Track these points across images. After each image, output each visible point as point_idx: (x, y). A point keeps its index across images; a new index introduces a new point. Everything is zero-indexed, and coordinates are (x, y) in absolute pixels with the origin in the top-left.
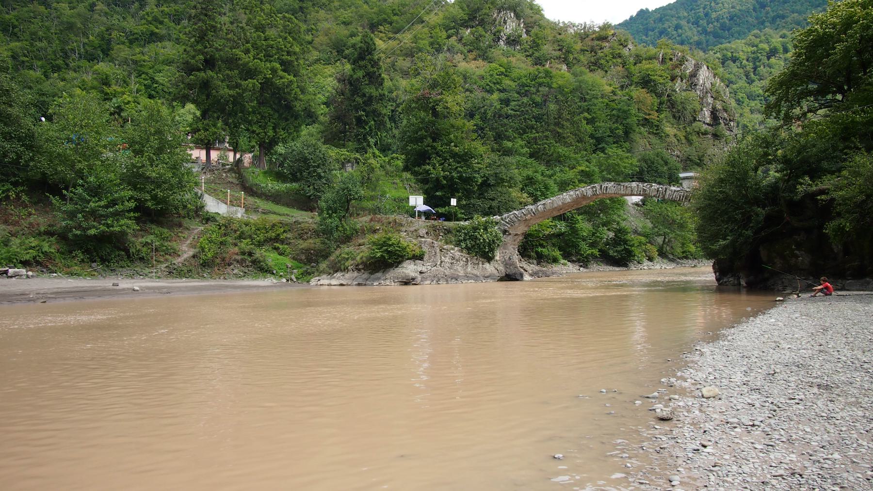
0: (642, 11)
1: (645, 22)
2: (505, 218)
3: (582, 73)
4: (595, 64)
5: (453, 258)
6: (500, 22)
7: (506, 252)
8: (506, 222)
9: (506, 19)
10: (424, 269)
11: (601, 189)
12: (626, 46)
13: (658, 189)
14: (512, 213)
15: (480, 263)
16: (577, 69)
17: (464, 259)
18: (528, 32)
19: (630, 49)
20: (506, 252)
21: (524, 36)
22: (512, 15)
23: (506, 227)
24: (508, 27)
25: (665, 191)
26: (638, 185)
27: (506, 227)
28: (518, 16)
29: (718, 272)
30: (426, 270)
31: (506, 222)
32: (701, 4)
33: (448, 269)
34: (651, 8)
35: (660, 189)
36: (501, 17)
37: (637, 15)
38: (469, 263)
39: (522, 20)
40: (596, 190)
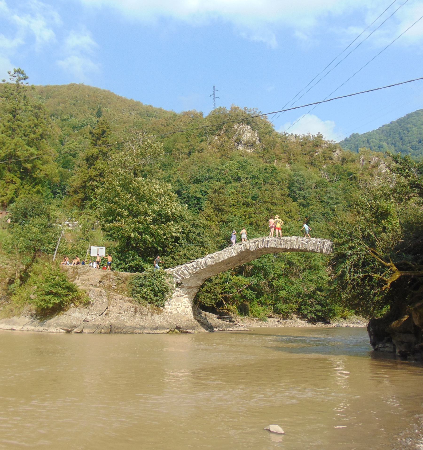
0: (353, 135)
1: (356, 143)
2: (177, 271)
3: (300, 170)
4: (312, 164)
5: (121, 308)
6: (239, 132)
7: (179, 305)
8: (178, 274)
9: (244, 130)
10: (89, 318)
11: (263, 243)
12: (335, 151)
13: (316, 242)
14: (184, 266)
15: (149, 314)
16: (297, 166)
17: (133, 310)
18: (260, 140)
19: (338, 154)
20: (179, 305)
21: (258, 143)
22: (249, 127)
23: (178, 280)
24: (246, 136)
25: (323, 245)
26: (297, 239)
27: (178, 280)
28: (253, 129)
29: (372, 335)
30: (90, 319)
31: (178, 274)
32: (397, 131)
33: (115, 319)
34: (361, 133)
35: (318, 243)
36: (241, 129)
37: (350, 137)
38: (138, 314)
39: (256, 131)
40: (258, 245)
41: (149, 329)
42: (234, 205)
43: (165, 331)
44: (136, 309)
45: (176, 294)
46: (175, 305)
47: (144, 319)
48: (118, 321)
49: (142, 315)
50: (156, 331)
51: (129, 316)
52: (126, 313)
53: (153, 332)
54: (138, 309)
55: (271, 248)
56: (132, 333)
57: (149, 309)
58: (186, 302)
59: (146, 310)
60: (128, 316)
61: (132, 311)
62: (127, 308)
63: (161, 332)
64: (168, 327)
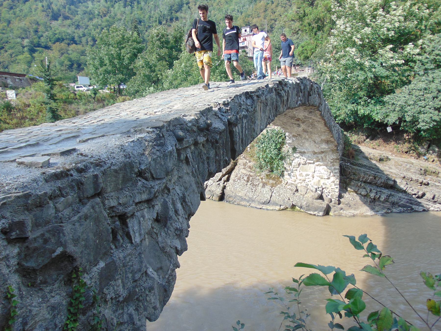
38: (249, 184)
41: (257, 203)
42: (233, 11)
43: (278, 208)
44: (248, 178)
45: (296, 161)
46: (301, 175)
47: (253, 191)
48: (412, 134)
49: (253, 185)
50: (264, 207)
51: (241, 185)
52: (239, 181)
53: (261, 207)
54: (251, 178)
55: (243, 151)
56: (238, 204)
57: (262, 179)
58: (323, 171)
59: (259, 179)
60: (240, 184)
61: (244, 180)
62: (241, 176)
63: (271, 208)
64: (281, 203)
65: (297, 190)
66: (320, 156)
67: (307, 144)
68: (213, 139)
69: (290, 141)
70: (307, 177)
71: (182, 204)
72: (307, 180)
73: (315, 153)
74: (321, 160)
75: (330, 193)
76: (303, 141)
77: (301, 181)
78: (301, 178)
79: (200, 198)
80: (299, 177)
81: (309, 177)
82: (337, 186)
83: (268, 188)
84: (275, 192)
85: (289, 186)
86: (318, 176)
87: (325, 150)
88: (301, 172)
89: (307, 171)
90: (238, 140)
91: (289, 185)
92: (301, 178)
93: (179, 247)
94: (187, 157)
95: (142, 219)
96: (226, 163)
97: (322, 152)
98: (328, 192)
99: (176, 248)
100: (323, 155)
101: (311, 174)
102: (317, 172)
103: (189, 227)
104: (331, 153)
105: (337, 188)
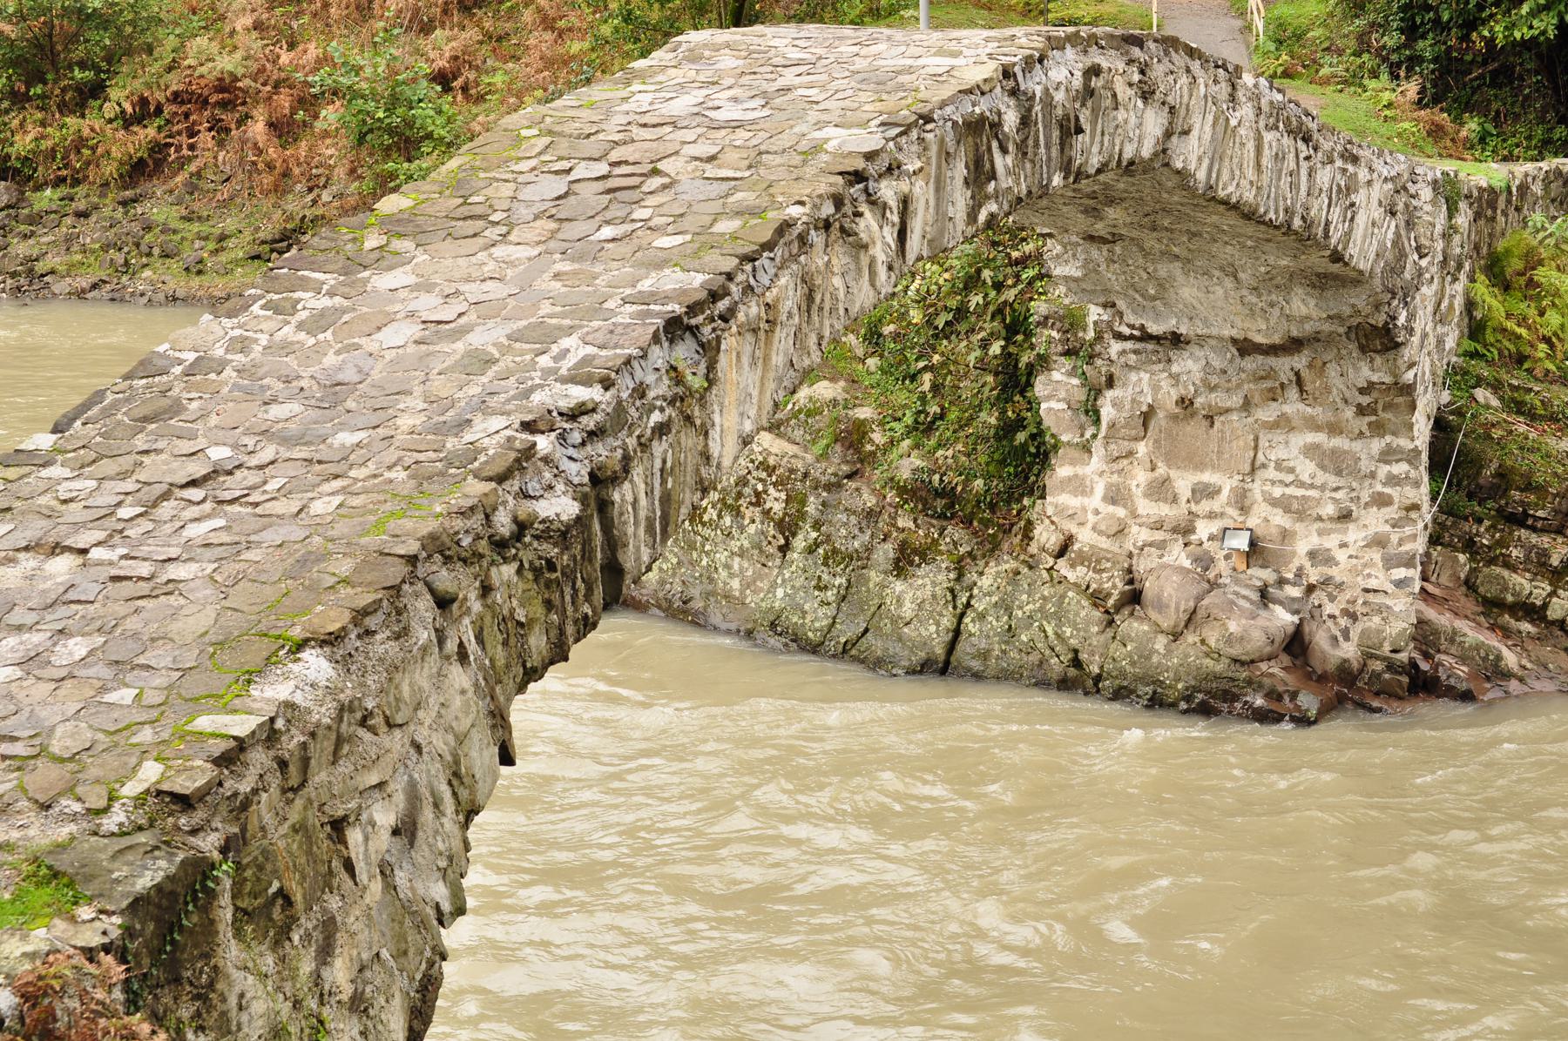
60: (734, 545)
65: (1134, 598)
66: (1284, 366)
67: (1188, 291)
68: (540, 558)
69: (1071, 270)
70: (1205, 506)
71: (450, 783)
72: (1204, 530)
73: (1245, 348)
74: (1293, 393)
75: (1353, 617)
76: (1163, 270)
77: (1159, 536)
78: (1164, 510)
79: (497, 759)
80: (1146, 507)
81: (1216, 505)
82: (1400, 573)
83: (930, 580)
84: (979, 605)
85: (1080, 570)
86: (1274, 503)
87: (1309, 328)
88: (1162, 469)
89: (1200, 466)
90: (630, 530)
91: (1082, 559)
92: (1164, 510)
93: (446, 907)
94: (461, 645)
95: (370, 829)
96: (585, 626)
97: (1293, 345)
98: (1345, 612)
99: (437, 907)
100: (1300, 361)
101: (1227, 484)
102: (1271, 473)
103: (467, 848)
104: (1353, 346)
105: (1400, 584)
